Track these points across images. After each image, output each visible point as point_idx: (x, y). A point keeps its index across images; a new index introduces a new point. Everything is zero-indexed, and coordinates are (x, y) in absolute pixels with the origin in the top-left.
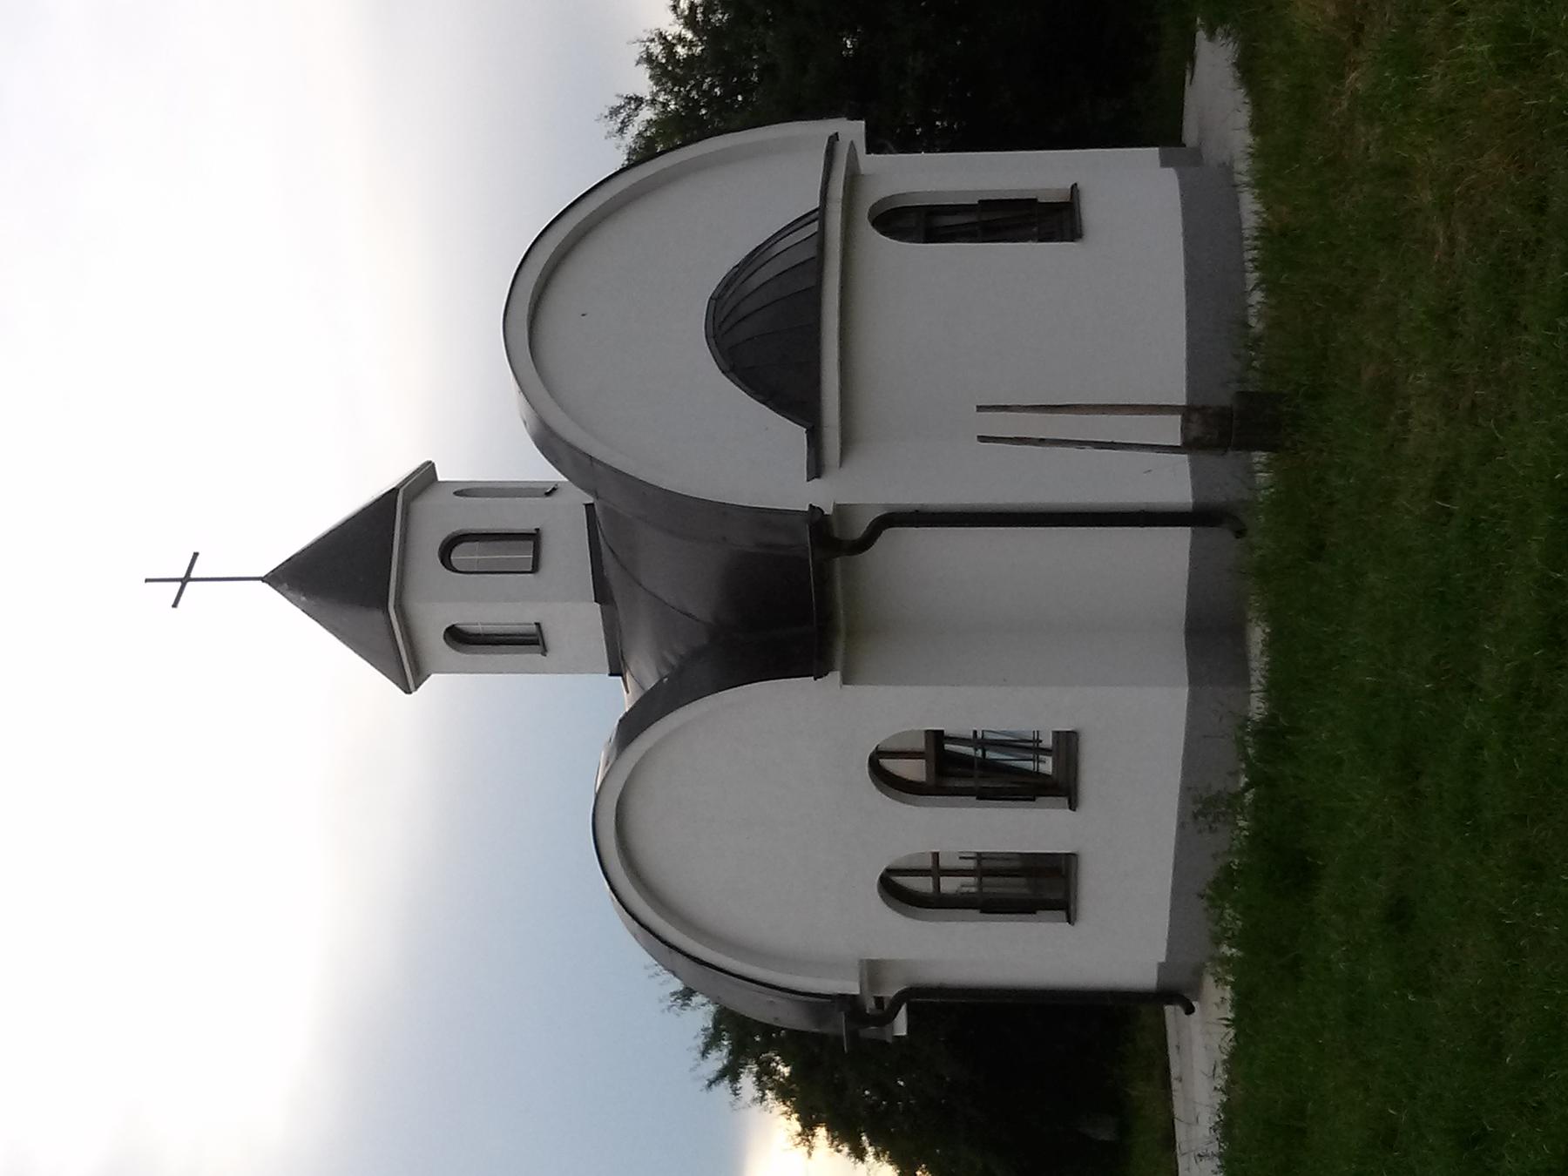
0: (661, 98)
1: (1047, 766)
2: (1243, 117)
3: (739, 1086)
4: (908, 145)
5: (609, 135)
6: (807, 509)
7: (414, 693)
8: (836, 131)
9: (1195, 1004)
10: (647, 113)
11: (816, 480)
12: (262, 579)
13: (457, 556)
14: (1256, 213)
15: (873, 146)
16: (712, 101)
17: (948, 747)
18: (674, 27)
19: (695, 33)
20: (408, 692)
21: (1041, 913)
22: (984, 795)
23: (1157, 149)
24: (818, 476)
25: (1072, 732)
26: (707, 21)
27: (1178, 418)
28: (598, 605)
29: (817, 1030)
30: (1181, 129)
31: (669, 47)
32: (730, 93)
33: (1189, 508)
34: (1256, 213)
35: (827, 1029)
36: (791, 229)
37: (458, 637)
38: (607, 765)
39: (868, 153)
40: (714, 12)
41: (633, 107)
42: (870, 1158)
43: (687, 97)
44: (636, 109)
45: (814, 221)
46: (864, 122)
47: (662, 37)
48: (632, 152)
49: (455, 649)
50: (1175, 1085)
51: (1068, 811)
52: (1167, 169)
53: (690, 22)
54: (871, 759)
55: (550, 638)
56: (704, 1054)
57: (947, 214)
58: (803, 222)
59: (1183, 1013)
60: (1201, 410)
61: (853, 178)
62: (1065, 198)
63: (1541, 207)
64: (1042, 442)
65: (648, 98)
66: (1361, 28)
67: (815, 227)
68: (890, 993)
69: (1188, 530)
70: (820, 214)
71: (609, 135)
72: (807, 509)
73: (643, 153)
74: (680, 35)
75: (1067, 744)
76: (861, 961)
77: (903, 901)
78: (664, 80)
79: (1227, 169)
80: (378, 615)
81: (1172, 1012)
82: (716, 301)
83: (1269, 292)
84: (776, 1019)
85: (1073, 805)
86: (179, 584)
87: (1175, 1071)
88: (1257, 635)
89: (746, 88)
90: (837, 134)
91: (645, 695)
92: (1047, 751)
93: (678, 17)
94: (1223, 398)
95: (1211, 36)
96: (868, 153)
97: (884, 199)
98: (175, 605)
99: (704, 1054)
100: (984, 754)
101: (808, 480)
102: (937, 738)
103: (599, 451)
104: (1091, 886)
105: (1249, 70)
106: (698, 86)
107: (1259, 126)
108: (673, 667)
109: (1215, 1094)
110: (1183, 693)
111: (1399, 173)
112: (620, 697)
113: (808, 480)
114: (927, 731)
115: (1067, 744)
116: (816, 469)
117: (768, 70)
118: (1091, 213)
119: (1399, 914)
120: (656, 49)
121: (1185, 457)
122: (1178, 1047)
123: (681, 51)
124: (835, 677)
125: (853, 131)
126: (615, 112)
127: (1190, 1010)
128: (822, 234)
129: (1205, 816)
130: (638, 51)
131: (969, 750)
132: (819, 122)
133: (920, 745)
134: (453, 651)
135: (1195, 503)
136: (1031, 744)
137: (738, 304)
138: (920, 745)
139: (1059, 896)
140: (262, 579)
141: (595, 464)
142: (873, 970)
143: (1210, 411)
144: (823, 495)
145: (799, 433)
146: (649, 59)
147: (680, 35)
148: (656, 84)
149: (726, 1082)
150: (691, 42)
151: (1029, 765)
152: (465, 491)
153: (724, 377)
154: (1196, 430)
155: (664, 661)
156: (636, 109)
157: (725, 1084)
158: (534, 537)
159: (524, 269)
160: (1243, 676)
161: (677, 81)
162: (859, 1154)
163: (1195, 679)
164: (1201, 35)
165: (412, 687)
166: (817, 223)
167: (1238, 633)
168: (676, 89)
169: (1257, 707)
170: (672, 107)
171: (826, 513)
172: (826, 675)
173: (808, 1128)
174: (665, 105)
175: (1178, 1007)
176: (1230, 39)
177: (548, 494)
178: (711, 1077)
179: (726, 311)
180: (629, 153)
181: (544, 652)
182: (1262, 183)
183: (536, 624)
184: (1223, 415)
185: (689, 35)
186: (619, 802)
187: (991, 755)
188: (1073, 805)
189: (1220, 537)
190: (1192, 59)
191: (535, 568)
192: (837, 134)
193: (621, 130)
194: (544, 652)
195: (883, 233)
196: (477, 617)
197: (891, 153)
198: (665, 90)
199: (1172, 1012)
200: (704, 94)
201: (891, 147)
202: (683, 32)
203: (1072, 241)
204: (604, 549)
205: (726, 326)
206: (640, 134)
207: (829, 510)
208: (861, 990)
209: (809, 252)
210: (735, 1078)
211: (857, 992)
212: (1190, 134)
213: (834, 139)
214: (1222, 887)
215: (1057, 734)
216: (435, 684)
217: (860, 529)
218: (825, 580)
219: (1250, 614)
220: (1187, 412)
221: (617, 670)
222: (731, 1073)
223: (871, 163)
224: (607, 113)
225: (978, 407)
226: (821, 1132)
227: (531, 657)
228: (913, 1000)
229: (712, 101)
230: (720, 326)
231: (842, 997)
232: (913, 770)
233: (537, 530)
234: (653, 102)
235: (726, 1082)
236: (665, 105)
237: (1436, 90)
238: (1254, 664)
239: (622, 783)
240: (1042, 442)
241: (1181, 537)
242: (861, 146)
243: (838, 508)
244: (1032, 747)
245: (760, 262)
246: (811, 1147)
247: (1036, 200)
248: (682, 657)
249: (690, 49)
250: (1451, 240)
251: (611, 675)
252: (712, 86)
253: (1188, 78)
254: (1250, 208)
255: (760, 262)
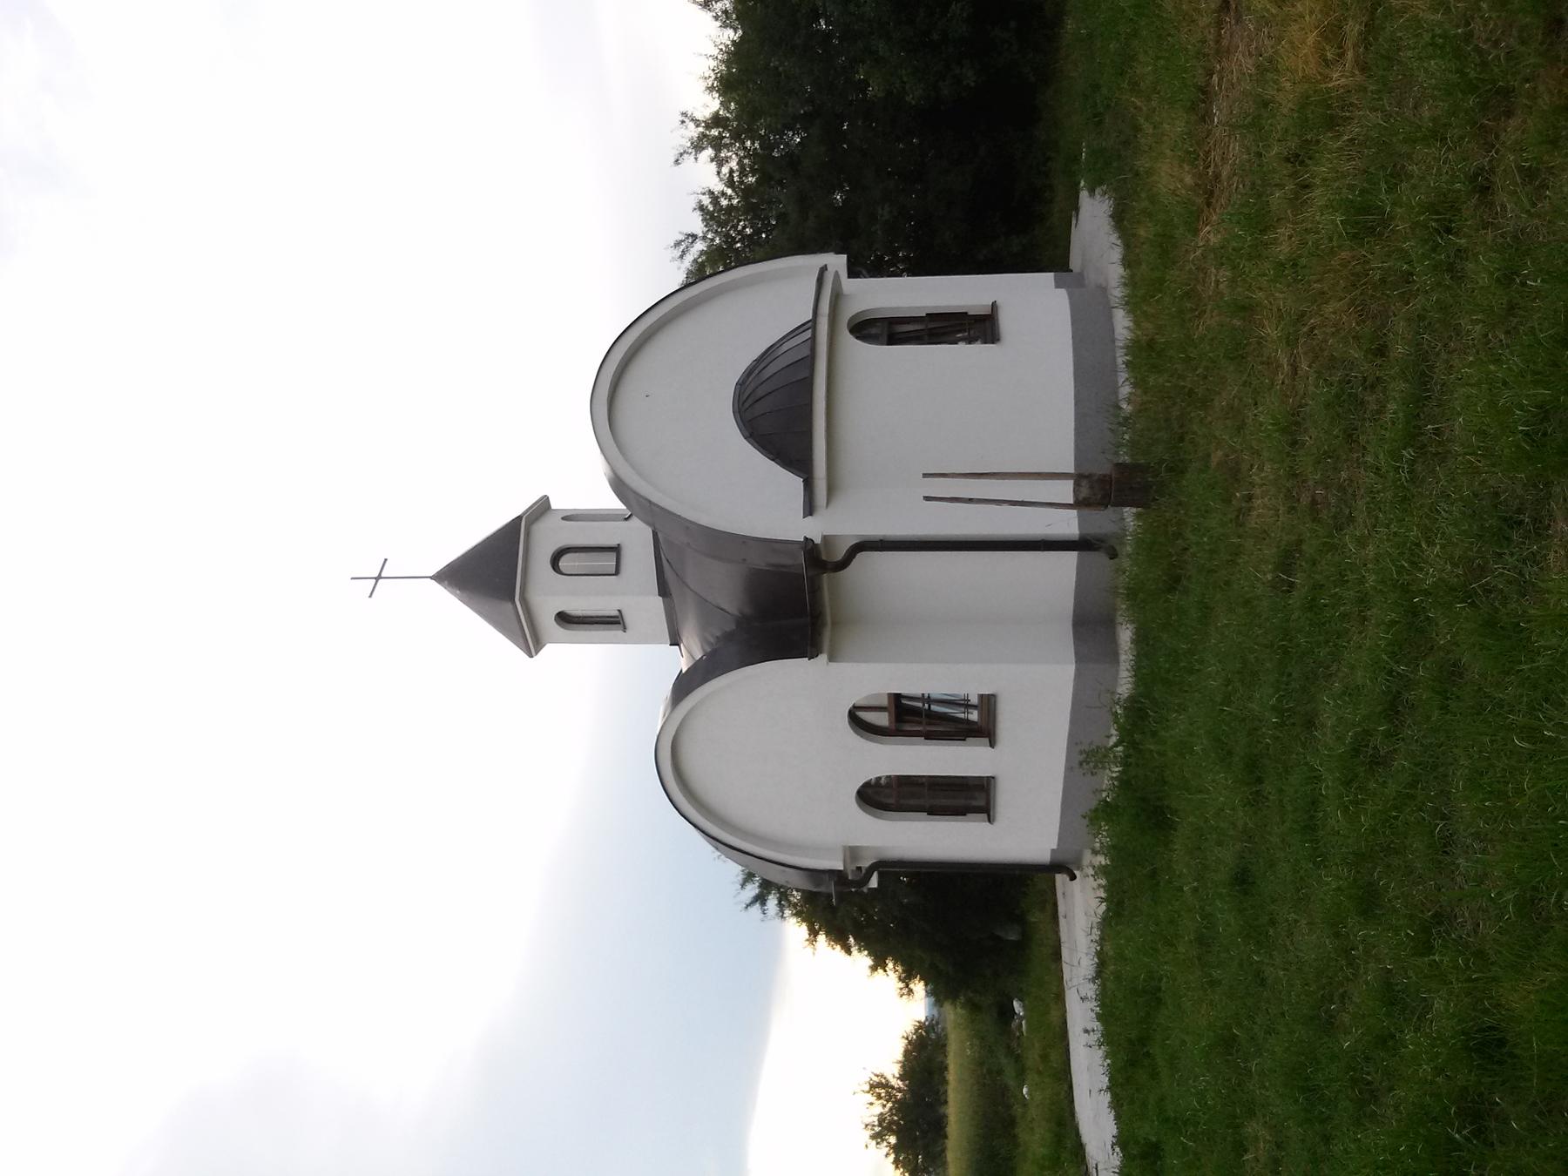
0: (709, 236)
1: (974, 716)
2: (1116, 254)
3: (766, 908)
4: (878, 269)
5: (673, 259)
6: (802, 540)
7: (535, 657)
8: (824, 263)
9: (1077, 873)
10: (700, 246)
11: (810, 517)
12: (431, 578)
13: (564, 563)
14: (1128, 328)
15: (852, 273)
16: (744, 238)
17: (904, 702)
18: (718, 186)
19: (733, 190)
20: (531, 656)
21: (970, 816)
22: (930, 736)
23: (1052, 274)
24: (811, 514)
25: (992, 695)
26: (741, 182)
27: (1072, 482)
28: (661, 598)
29: (815, 890)
30: (1068, 257)
31: (715, 199)
32: (757, 232)
33: (1076, 538)
34: (1128, 328)
35: (822, 889)
36: (794, 334)
37: (564, 619)
38: (664, 715)
39: (849, 277)
40: (746, 176)
41: (690, 241)
42: (854, 950)
43: (727, 235)
44: (692, 243)
45: (808, 329)
46: (846, 256)
47: (711, 193)
48: (689, 273)
49: (562, 627)
50: (1062, 921)
51: (988, 823)
52: (1059, 290)
53: (730, 183)
54: (850, 712)
55: (628, 619)
56: (743, 886)
57: (904, 323)
58: (801, 329)
59: (1068, 879)
60: (1088, 477)
61: (837, 297)
62: (988, 311)
63: (1382, 351)
64: (970, 501)
65: (701, 235)
66: (1212, 193)
67: (808, 334)
68: (866, 864)
69: (1075, 554)
70: (812, 324)
71: (673, 259)
72: (802, 540)
73: (698, 274)
74: (723, 191)
75: (988, 704)
76: (844, 847)
77: (871, 806)
78: (711, 223)
79: (1103, 290)
80: (509, 606)
81: (1061, 879)
82: (741, 384)
83: (1135, 385)
84: (787, 882)
85: (992, 745)
86: (383, 575)
87: (1061, 909)
88: (1125, 635)
89: (767, 227)
90: (826, 265)
91: (694, 664)
92: (974, 707)
93: (721, 180)
94: (1103, 467)
95: (1092, 192)
96: (849, 277)
97: (858, 313)
98: (370, 596)
99: (743, 886)
100: (929, 706)
101: (804, 517)
102: (897, 698)
103: (656, 497)
104: (1004, 799)
105: (1120, 219)
106: (735, 227)
107: (1127, 262)
108: (712, 644)
109: (1092, 944)
110: (1070, 669)
111: (1246, 309)
112: (678, 660)
113: (804, 517)
114: (889, 694)
115: (988, 704)
116: (810, 509)
117: (781, 217)
118: (1007, 323)
119: (1243, 880)
120: (706, 201)
121: (1075, 511)
122: (1064, 894)
123: (724, 202)
124: (823, 658)
125: (837, 262)
126: (678, 244)
127: (1073, 877)
128: (813, 338)
129: (1088, 763)
130: (692, 202)
131: (920, 705)
132: (812, 256)
133: (885, 702)
134: (562, 629)
135: (1080, 534)
136: (963, 702)
137: (757, 388)
138: (885, 702)
139: (981, 803)
140: (431, 578)
141: (653, 507)
142: (852, 853)
143: (1096, 478)
144: (813, 529)
145: (798, 482)
146: (701, 208)
147: (723, 191)
148: (706, 226)
149: (757, 905)
150: (731, 196)
151: (962, 716)
152: (569, 517)
153: (745, 441)
154: (1085, 492)
155: (704, 650)
156: (692, 243)
157: (757, 906)
158: (616, 550)
159: (606, 363)
160: (1114, 656)
161: (720, 224)
162: (849, 952)
163: (1080, 658)
164: (1084, 194)
165: (533, 653)
166: (810, 330)
167: (1109, 624)
168: (719, 230)
169: (1125, 686)
170: (717, 242)
171: (816, 542)
172: (817, 656)
173: (814, 933)
174: (712, 240)
175: (1065, 876)
176: (1107, 196)
177: (626, 519)
178: (748, 902)
179: (747, 394)
180: (687, 274)
181: (625, 629)
182: (1133, 305)
183: (619, 611)
184: (1104, 481)
185: (729, 192)
186: (673, 743)
187: (934, 708)
188: (992, 745)
189: (1098, 559)
190: (1077, 209)
191: (617, 572)
192: (826, 265)
193: (681, 257)
194: (625, 629)
195: (857, 338)
196: (576, 607)
197: (865, 277)
198: (712, 231)
199: (1061, 879)
200: (739, 233)
201: (864, 272)
202: (725, 188)
203: (993, 343)
204: (664, 561)
205: (747, 405)
206: (695, 261)
207: (818, 540)
208: (845, 866)
209: (806, 352)
210: (763, 903)
211: (842, 868)
212: (1075, 262)
213: (824, 269)
214: (1103, 813)
215: (981, 697)
216: (549, 650)
217: (840, 554)
218: (815, 590)
219: (1120, 619)
220: (1079, 478)
221: (675, 641)
222: (760, 899)
223: (851, 285)
224: (672, 244)
225: (924, 474)
226: (822, 938)
227: (616, 632)
228: (881, 869)
229: (744, 238)
230: (743, 404)
231: (832, 872)
232: (882, 719)
233: (619, 545)
234: (704, 238)
235: (757, 905)
236: (712, 240)
237: (1284, 250)
238: (1123, 657)
239: (675, 729)
240: (970, 501)
241: (1071, 557)
242: (844, 273)
243: (825, 538)
244: (965, 704)
245: (769, 359)
246: (815, 949)
247: (966, 313)
248: (717, 637)
249: (730, 200)
250: (1295, 369)
251: (671, 645)
252: (744, 227)
253: (1074, 222)
254: (1122, 323)
255: (769, 359)
